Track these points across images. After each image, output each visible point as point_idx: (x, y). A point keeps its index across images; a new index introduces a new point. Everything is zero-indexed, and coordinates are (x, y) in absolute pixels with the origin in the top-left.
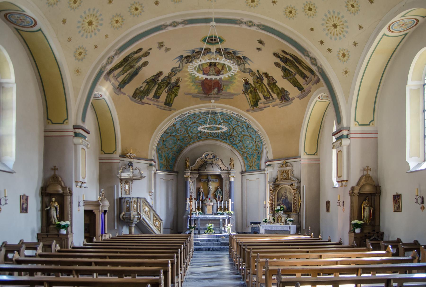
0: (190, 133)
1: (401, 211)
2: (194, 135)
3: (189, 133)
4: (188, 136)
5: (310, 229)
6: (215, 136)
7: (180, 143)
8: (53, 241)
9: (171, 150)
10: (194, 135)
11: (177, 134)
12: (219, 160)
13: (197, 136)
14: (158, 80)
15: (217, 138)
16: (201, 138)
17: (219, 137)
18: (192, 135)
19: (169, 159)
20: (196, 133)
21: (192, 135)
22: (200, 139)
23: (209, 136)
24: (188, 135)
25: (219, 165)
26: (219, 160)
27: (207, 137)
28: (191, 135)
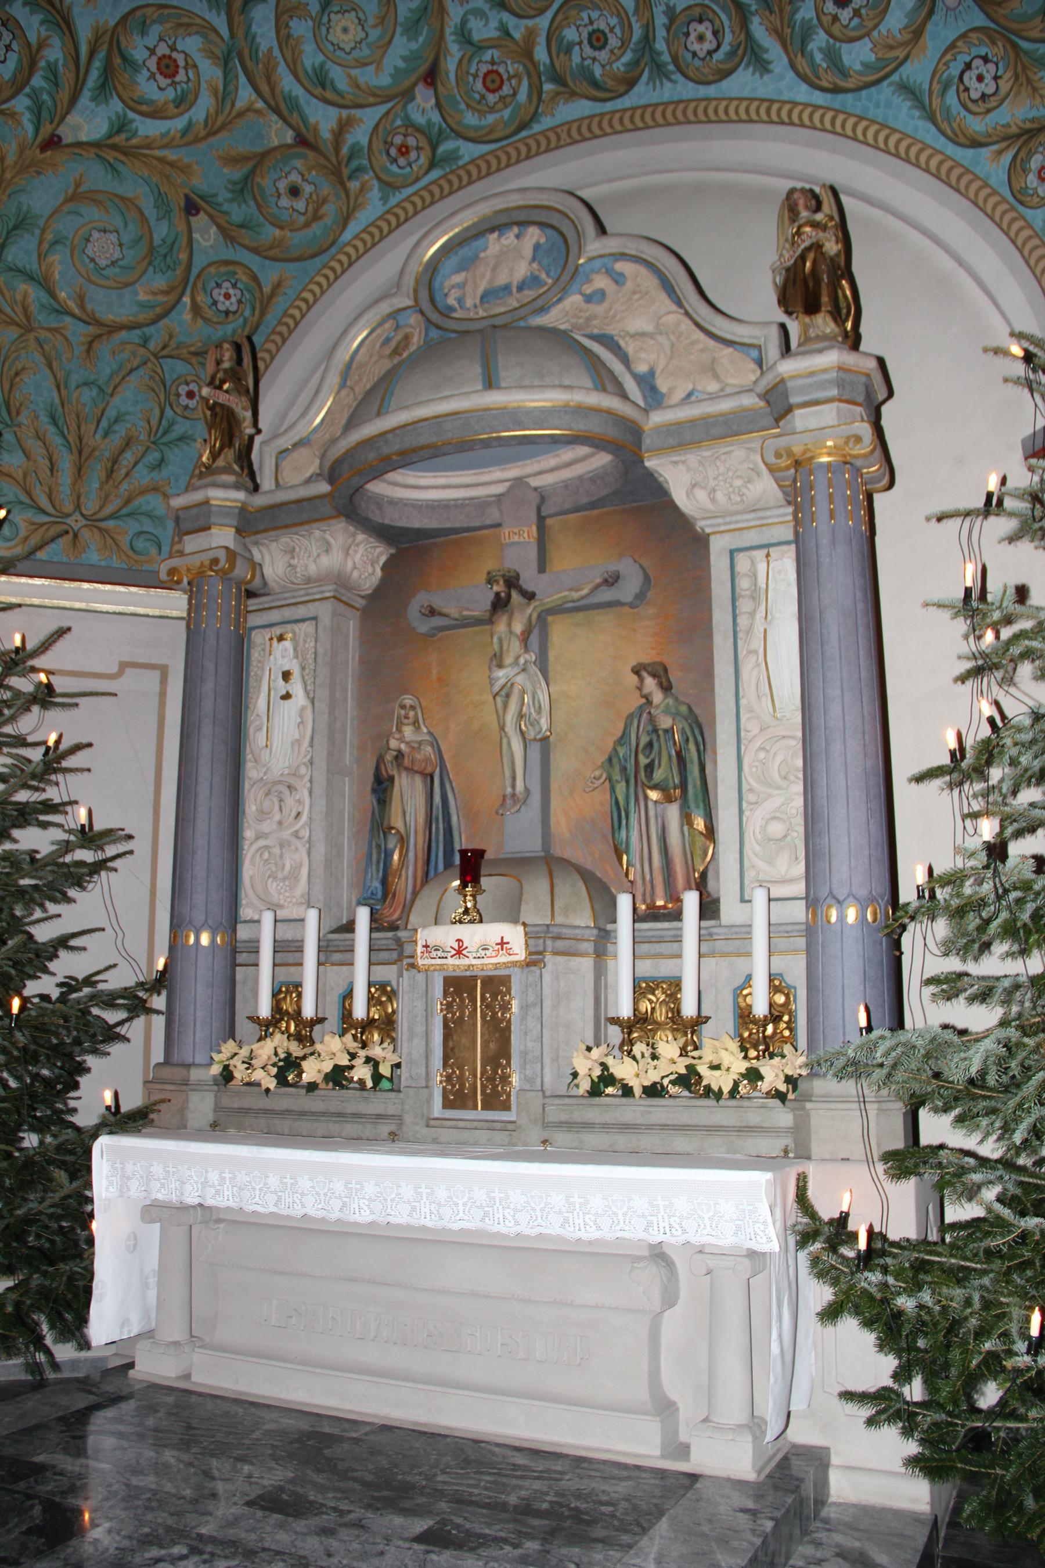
0: (298, 91)
1: (828, 1449)
2: (370, 117)
3: (294, 105)
4: (302, 141)
5: (449, 1532)
6: (619, 66)
7: (229, 253)
8: (1031, 1309)
9: (145, 342)
10: (370, 117)
11: (148, 128)
12: (618, 279)
13: (410, 124)
14: (589, 281)
15: (643, 94)
16: (469, 151)
17: (659, 71)
18: (343, 127)
19: (116, 439)
20: (380, 97)
21: (343, 127)
22: (452, 156)
23: (548, 87)
24: (289, 136)
25: (630, 347)
26: (618, 279)
27: (535, 117)
28: (326, 132)
